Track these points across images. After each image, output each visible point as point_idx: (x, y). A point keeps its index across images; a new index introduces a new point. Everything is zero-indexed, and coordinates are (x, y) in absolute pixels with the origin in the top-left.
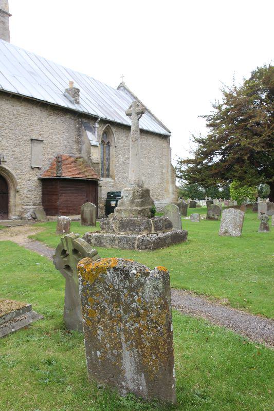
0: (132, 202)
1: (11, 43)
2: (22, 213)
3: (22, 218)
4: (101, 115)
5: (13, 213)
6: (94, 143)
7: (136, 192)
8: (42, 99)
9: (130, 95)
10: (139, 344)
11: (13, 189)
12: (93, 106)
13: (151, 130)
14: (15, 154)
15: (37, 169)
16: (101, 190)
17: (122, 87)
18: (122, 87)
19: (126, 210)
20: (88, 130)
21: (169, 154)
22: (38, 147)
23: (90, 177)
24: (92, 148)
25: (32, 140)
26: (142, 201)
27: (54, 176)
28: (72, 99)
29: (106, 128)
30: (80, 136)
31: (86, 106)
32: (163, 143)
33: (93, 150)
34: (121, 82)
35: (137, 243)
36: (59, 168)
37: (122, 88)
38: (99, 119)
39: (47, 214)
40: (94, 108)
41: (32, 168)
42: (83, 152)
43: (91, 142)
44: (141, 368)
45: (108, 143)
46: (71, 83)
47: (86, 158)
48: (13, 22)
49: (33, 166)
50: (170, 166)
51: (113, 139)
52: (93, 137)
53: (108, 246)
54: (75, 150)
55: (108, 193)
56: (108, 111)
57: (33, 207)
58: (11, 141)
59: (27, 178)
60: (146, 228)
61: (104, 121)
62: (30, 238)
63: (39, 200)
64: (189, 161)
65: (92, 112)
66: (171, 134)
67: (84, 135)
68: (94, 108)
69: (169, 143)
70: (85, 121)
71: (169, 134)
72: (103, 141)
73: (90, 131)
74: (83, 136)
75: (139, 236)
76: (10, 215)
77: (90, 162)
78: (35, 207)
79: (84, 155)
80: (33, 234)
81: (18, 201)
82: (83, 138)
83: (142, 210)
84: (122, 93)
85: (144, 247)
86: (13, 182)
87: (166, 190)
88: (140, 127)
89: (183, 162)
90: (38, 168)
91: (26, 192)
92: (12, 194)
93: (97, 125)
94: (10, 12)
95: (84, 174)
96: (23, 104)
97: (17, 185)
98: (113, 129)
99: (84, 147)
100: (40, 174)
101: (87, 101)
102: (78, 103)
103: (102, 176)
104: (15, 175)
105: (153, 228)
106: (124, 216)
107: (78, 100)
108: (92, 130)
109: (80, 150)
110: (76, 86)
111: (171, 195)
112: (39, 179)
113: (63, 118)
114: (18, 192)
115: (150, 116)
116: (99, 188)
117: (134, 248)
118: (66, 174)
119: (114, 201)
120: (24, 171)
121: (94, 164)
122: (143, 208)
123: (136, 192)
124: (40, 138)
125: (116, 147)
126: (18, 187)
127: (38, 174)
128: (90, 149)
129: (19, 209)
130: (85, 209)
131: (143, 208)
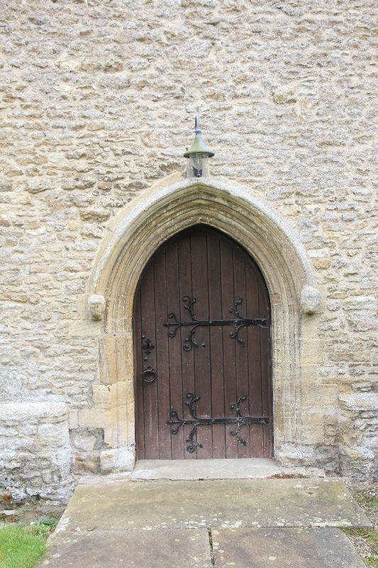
11: (285, 296)
14: (293, 114)
21: (266, 300)
58: (265, 47)
86: (282, 265)
88: (306, 311)
92: (283, 325)
97: (304, 279)
120: (350, 199)
126: (311, 293)
129: (322, 408)
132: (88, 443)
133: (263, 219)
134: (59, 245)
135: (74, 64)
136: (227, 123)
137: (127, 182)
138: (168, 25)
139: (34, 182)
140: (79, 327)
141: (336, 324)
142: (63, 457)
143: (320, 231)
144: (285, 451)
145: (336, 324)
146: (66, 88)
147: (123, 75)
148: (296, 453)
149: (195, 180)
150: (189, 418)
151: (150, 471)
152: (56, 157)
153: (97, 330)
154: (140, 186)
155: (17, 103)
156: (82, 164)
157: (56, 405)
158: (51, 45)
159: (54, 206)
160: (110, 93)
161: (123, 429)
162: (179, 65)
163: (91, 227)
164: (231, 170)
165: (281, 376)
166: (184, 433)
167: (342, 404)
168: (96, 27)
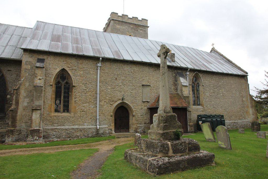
1: (149, 38)
4: (190, 66)
5: (131, 128)
6: (185, 84)
7: (160, 118)
8: (149, 61)
9: (218, 54)
13: (230, 72)
15: (147, 102)
17: (213, 50)
18: (213, 50)
19: (154, 133)
20: (181, 77)
23: (180, 106)
24: (183, 87)
25: (143, 85)
26: (165, 125)
29: (195, 74)
30: (176, 81)
32: (242, 81)
33: (184, 89)
34: (212, 47)
37: (213, 51)
38: (189, 70)
41: (144, 102)
42: (178, 90)
43: (183, 84)
47: (180, 94)
48: (149, 30)
49: (144, 101)
50: (248, 96)
51: (200, 81)
54: (173, 90)
55: (198, 116)
56: (197, 64)
57: (144, 125)
58: (130, 87)
59: (140, 108)
61: (192, 70)
66: (248, 74)
67: (179, 80)
69: (247, 80)
70: (180, 71)
71: (246, 74)
74: (178, 80)
76: (130, 130)
77: (182, 96)
78: (145, 125)
82: (178, 82)
83: (164, 133)
84: (213, 54)
87: (247, 112)
89: (263, 92)
90: (147, 101)
91: (139, 116)
92: (131, 117)
93: (188, 73)
94: (148, 26)
95: (176, 104)
96: (137, 66)
97: (133, 112)
98: (201, 75)
99: (179, 87)
100: (149, 105)
102: (174, 61)
104: (132, 106)
107: (174, 60)
109: (177, 89)
111: (252, 115)
112: (148, 108)
114: (134, 116)
119: (201, 121)
121: (185, 98)
123: (160, 118)
124: (148, 84)
125: (203, 86)
126: (134, 114)
127: (148, 105)
128: (182, 88)
129: (135, 126)
131: (165, 131)
132: (110, 130)
133: (129, 105)
134: (107, 108)
135: (110, 88)
136: (126, 95)
137: (115, 101)
138: (120, 84)
139: (105, 100)
140: (109, 117)
141: (136, 117)
142: (108, 132)
143: (135, 107)
144: (131, 131)
145: (136, 117)
146: (109, 90)
147: (115, 89)
148: (132, 131)
149: (123, 101)
150: (120, 128)
151: (116, 134)
152: (107, 98)
153: (111, 118)
154: (116, 101)
155: (104, 92)
156: (110, 99)
157: (107, 126)
158: (108, 85)
159: (107, 103)
160: (114, 91)
161: (113, 129)
162: (121, 88)
163: (111, 106)
164: (126, 100)
165: (130, 123)
166: (119, 130)
167: (137, 126)
168: (113, 84)
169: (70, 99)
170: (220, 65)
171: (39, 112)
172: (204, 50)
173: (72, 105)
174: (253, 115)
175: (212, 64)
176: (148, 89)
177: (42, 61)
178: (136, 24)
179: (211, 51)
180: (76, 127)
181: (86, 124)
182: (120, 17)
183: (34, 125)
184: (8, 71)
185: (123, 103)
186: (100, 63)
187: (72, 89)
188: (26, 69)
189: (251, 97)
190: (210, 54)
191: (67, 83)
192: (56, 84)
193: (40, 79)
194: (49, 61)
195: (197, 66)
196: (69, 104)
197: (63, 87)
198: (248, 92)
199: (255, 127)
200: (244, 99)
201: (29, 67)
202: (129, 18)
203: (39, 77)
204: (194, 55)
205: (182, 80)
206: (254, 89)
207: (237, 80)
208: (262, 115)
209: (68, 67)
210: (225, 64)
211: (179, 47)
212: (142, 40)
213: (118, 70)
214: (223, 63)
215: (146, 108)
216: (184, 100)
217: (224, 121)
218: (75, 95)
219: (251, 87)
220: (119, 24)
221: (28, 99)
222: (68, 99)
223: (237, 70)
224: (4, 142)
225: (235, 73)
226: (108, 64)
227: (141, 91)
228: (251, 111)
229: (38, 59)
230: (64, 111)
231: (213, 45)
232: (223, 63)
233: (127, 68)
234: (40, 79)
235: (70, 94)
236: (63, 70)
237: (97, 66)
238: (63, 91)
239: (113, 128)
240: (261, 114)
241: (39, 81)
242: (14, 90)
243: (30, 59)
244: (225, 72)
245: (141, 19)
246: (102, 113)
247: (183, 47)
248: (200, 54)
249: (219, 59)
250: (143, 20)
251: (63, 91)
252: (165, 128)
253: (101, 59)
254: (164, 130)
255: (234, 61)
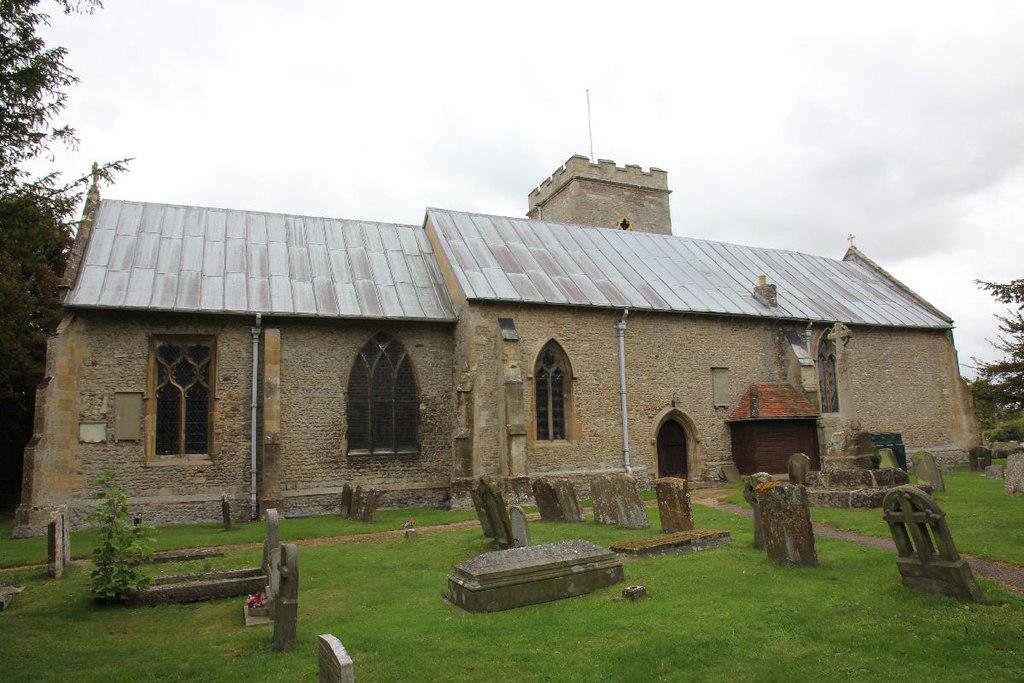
0: (845, 448)
1: (677, 228)
2: (706, 472)
3: (706, 479)
6: (806, 362)
10: (794, 532)
12: (796, 302)
13: (908, 323)
16: (823, 434)
17: (852, 255)
18: (852, 255)
19: (839, 461)
22: (721, 379)
23: (802, 415)
25: (713, 369)
27: (748, 417)
28: (765, 301)
30: (782, 353)
31: (792, 305)
32: (940, 342)
33: (805, 373)
35: (851, 499)
36: (753, 405)
37: (852, 257)
39: (742, 472)
40: (801, 306)
43: (801, 361)
44: (796, 546)
45: (831, 357)
46: (763, 278)
48: (675, 203)
52: (802, 354)
53: (816, 505)
60: (863, 482)
62: (720, 500)
63: (728, 453)
64: (1003, 368)
65: (797, 315)
68: (801, 306)
72: (821, 356)
73: (798, 345)
75: (855, 491)
76: (690, 475)
79: (792, 381)
80: (724, 497)
81: (699, 455)
84: (853, 265)
85: (860, 504)
87: (956, 426)
89: (991, 370)
92: (691, 445)
93: (809, 333)
99: (791, 370)
100: (727, 416)
101: (791, 298)
102: (775, 305)
103: (825, 410)
105: (874, 482)
106: (836, 468)
108: (801, 343)
109: (785, 375)
110: (769, 282)
112: (727, 423)
113: (754, 332)
115: (908, 299)
116: (819, 431)
117: (848, 506)
118: (764, 414)
122: (859, 456)
124: (724, 365)
129: (702, 466)
130: (794, 462)
131: (859, 456)
135: (645, 378)
157: (643, 468)
159: (642, 415)
163: (650, 420)
169: (565, 406)
170: (879, 302)
171: (522, 439)
172: (828, 257)
173: (572, 422)
174: (971, 431)
175: (858, 300)
176: (724, 376)
177: (507, 324)
178: (636, 187)
179: (846, 258)
180: (584, 471)
181: (602, 464)
182: (594, 170)
183: (515, 467)
184: (417, 346)
185: (675, 412)
186: (624, 322)
187: (570, 386)
188: (479, 345)
189: (964, 381)
190: (844, 265)
191: (557, 371)
192: (536, 376)
193: (513, 367)
194: (522, 321)
195: (826, 311)
196: (566, 421)
197: (549, 380)
198: (956, 372)
199: (979, 459)
200: (946, 392)
201: (483, 339)
202: (619, 170)
203: (512, 363)
204: (808, 275)
205: (797, 350)
206: (972, 363)
207: (927, 342)
208: (993, 432)
209: (560, 335)
210: (889, 296)
211: (765, 252)
212: (657, 237)
213: (659, 334)
214: (886, 294)
215: (722, 422)
216: (806, 401)
217: (903, 447)
218: (579, 399)
219: (963, 356)
220: (594, 190)
221: (487, 412)
222: (543, 406)
223: (924, 312)
224: (449, 508)
225: (921, 324)
226: (638, 324)
227: (709, 381)
228: (965, 421)
229: (500, 320)
230: (555, 438)
231: (851, 238)
232: (886, 294)
233: (677, 330)
234: (513, 367)
235: (565, 396)
236: (552, 343)
237: (618, 330)
238: (550, 392)
239: (655, 471)
240: (988, 432)
241: (512, 372)
242: (460, 392)
243: (484, 322)
244: (896, 323)
245: (648, 171)
246: (634, 439)
247: (775, 251)
248: (822, 269)
249: (871, 281)
250: (655, 174)
251: (550, 392)
252: (859, 451)
253: (627, 312)
254: (857, 454)
255: (913, 288)
